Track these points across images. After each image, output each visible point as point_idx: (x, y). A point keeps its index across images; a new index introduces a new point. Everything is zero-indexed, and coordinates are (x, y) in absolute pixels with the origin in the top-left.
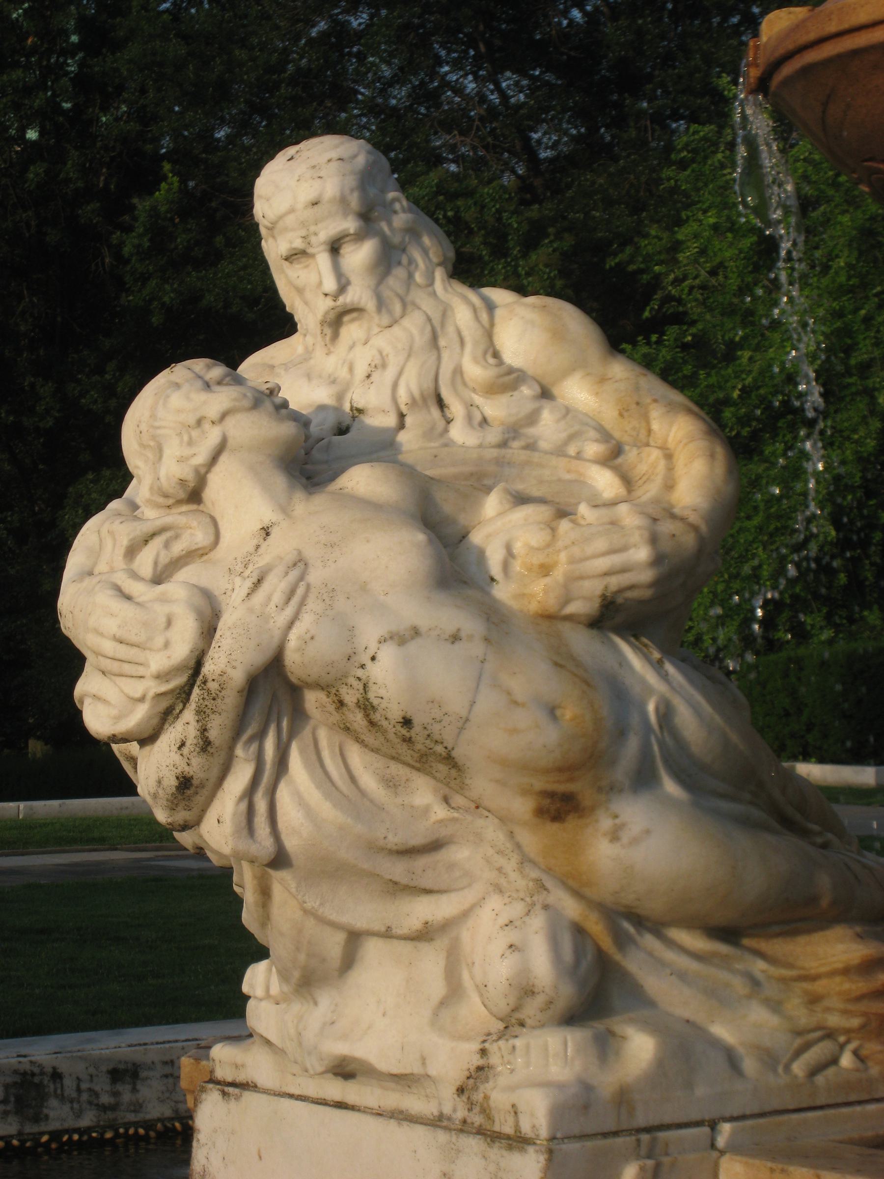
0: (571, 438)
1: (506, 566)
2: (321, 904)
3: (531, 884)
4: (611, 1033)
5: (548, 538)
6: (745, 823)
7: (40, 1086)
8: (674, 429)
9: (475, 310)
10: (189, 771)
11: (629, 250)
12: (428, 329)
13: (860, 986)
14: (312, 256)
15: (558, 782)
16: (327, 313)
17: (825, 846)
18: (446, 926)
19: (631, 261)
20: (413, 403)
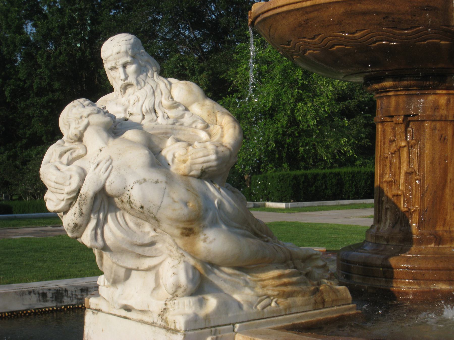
0: (194, 122)
1: (173, 160)
2: (118, 261)
3: (180, 255)
4: (204, 298)
5: (185, 152)
6: (244, 236)
7: (62, 293)
8: (224, 120)
9: (166, 85)
10: (77, 222)
11: (225, 74)
12: (152, 90)
13: (277, 282)
14: (117, 69)
15: (188, 225)
16: (122, 85)
17: (267, 241)
18: (155, 267)
19: (226, 77)
20: (147, 112)
